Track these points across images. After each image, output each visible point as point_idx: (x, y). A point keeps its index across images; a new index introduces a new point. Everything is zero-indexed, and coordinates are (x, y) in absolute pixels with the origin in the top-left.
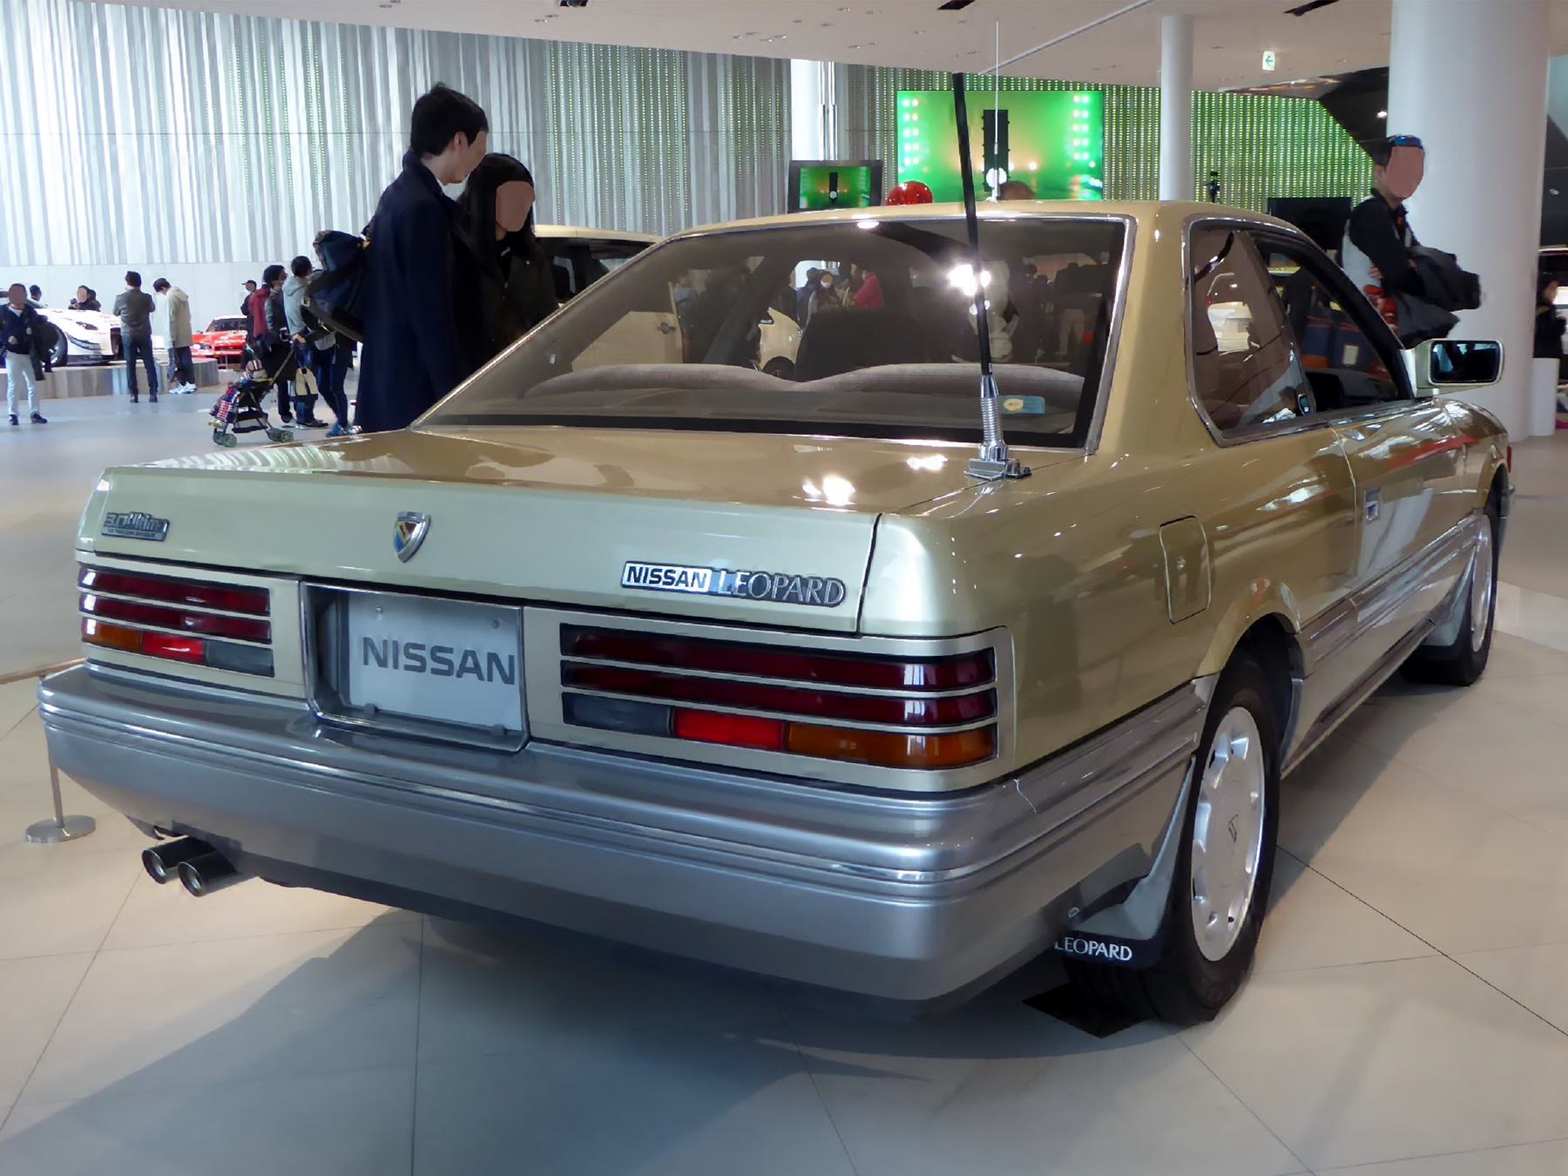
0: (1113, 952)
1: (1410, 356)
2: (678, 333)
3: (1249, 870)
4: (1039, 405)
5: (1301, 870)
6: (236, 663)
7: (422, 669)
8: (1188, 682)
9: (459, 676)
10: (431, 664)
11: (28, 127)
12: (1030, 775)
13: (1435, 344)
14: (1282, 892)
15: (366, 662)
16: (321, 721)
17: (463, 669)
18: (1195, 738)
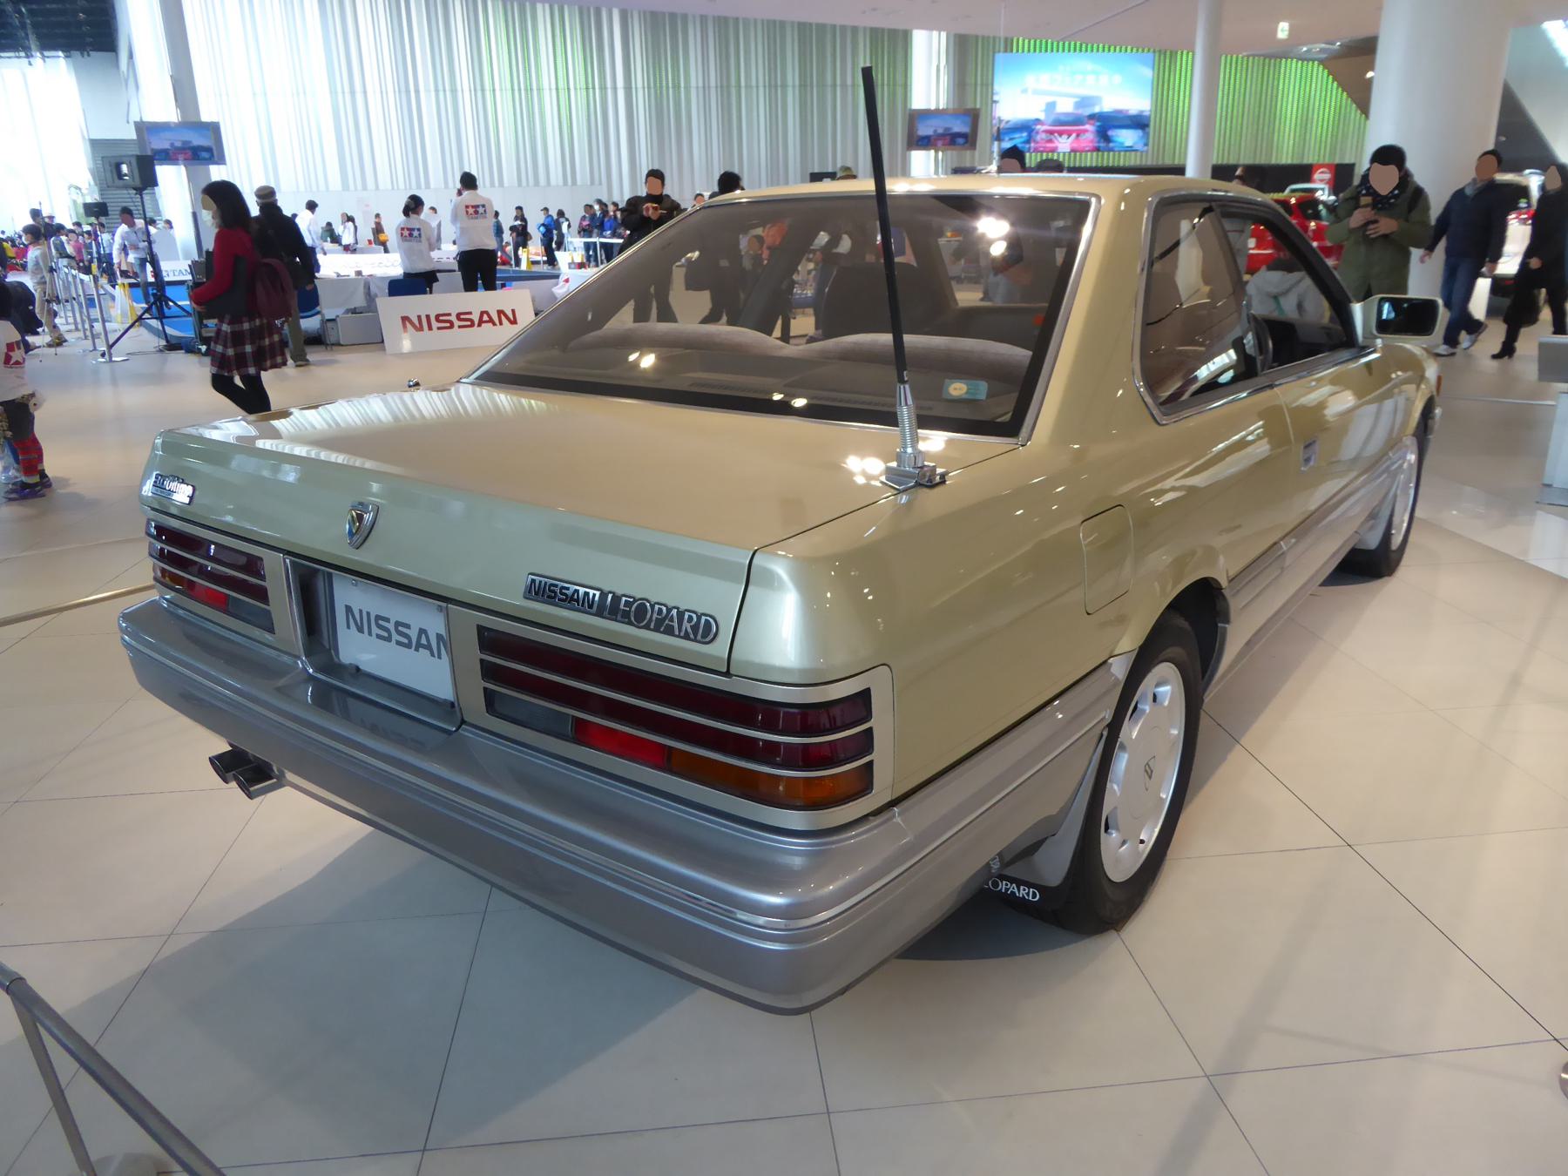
0: (1022, 892)
1: (1357, 309)
3: (1163, 796)
4: (982, 388)
5: (1229, 749)
9: (417, 650)
11: (358, 88)
12: (906, 804)
13: (1382, 300)
14: (1200, 787)
16: (311, 678)
17: (419, 646)
18: (1108, 715)
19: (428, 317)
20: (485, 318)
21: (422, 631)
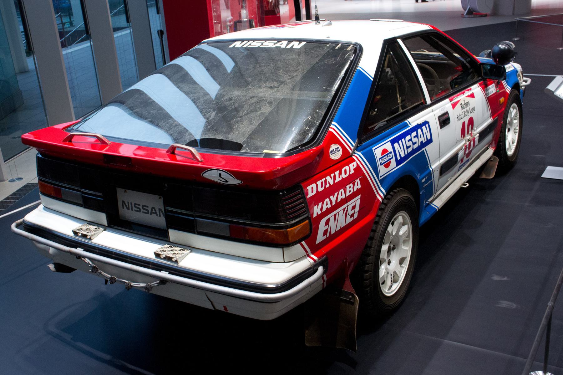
2: (167, 160)
6: (100, 263)
7: (140, 211)
8: (126, 12)
9: (151, 214)
10: (142, 210)
17: (152, 213)
19: (131, 203)
20: (154, 211)
21: (153, 208)
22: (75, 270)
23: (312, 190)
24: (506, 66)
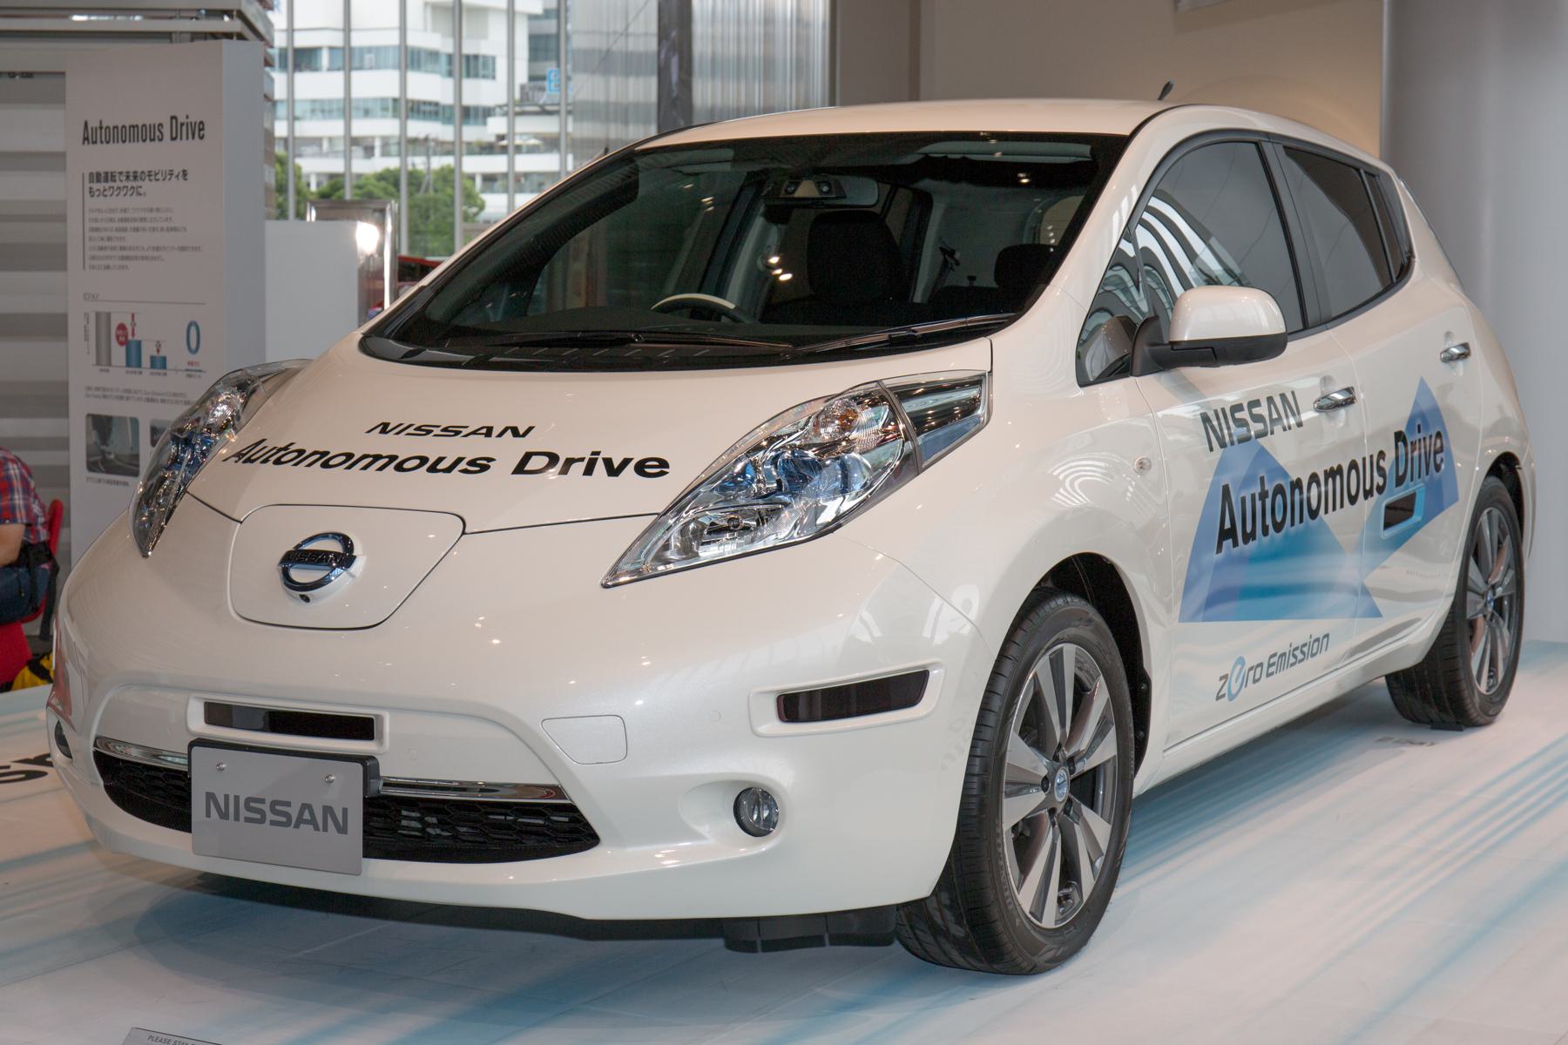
9: (297, 826)
10: (270, 816)
15: (345, 811)
17: (300, 821)
19: (237, 798)
20: (307, 816)
22: (1422, 381)
23: (927, 634)
24: (927, 634)
